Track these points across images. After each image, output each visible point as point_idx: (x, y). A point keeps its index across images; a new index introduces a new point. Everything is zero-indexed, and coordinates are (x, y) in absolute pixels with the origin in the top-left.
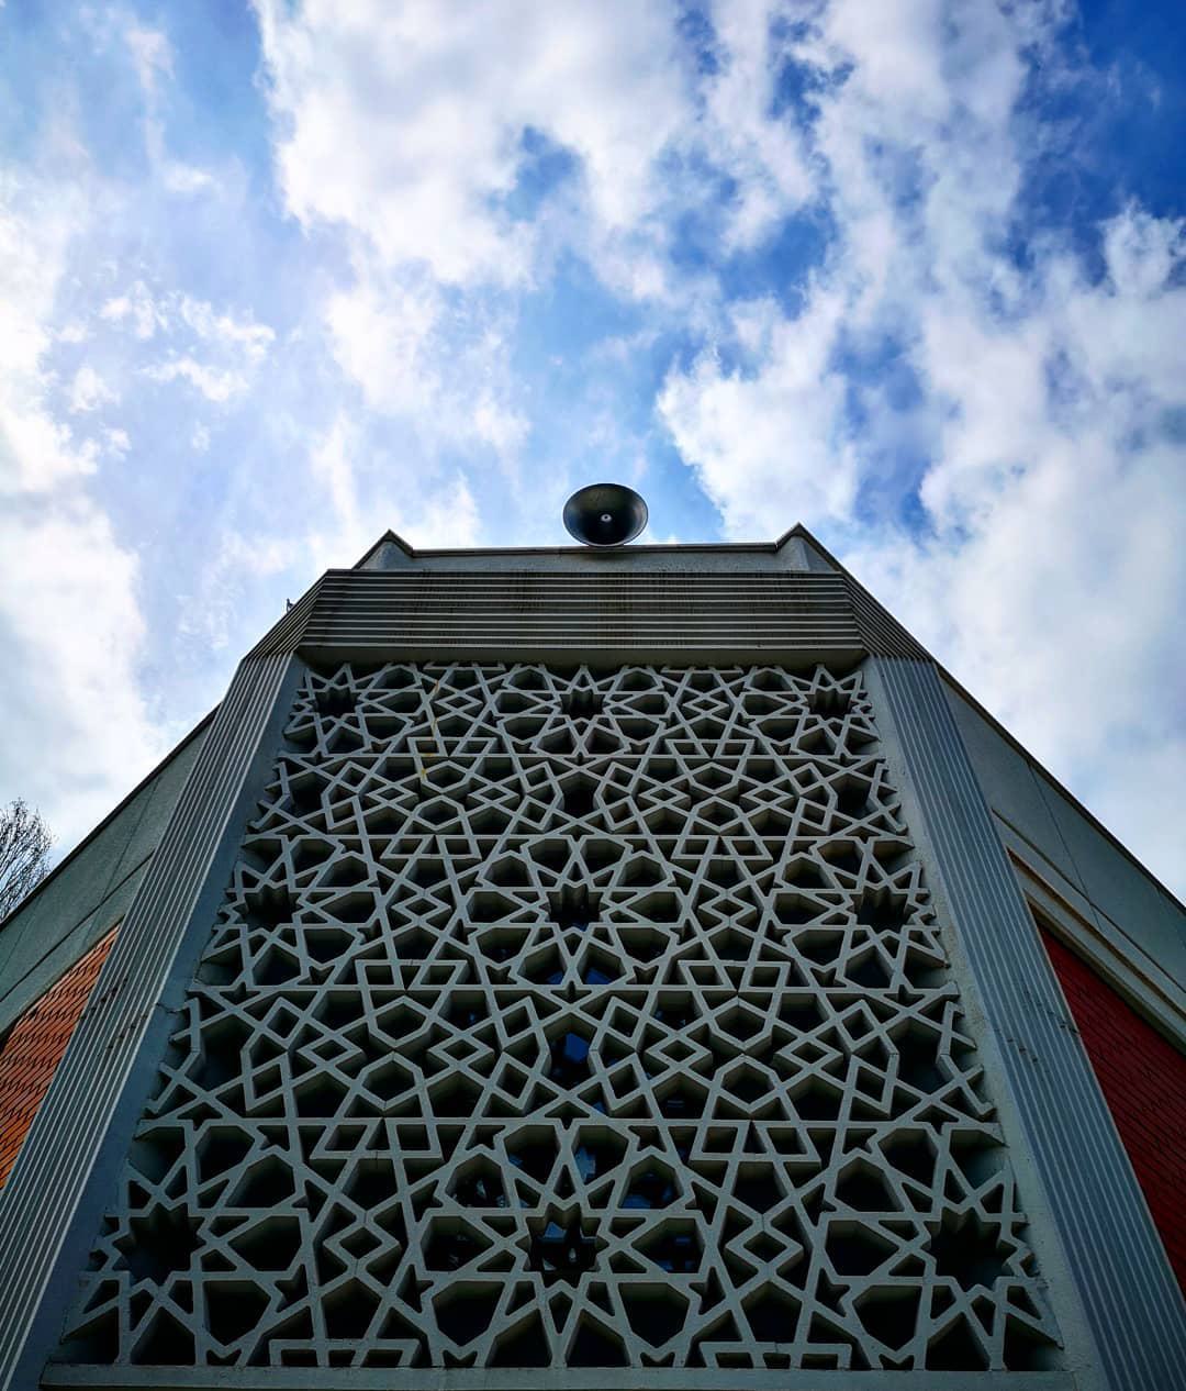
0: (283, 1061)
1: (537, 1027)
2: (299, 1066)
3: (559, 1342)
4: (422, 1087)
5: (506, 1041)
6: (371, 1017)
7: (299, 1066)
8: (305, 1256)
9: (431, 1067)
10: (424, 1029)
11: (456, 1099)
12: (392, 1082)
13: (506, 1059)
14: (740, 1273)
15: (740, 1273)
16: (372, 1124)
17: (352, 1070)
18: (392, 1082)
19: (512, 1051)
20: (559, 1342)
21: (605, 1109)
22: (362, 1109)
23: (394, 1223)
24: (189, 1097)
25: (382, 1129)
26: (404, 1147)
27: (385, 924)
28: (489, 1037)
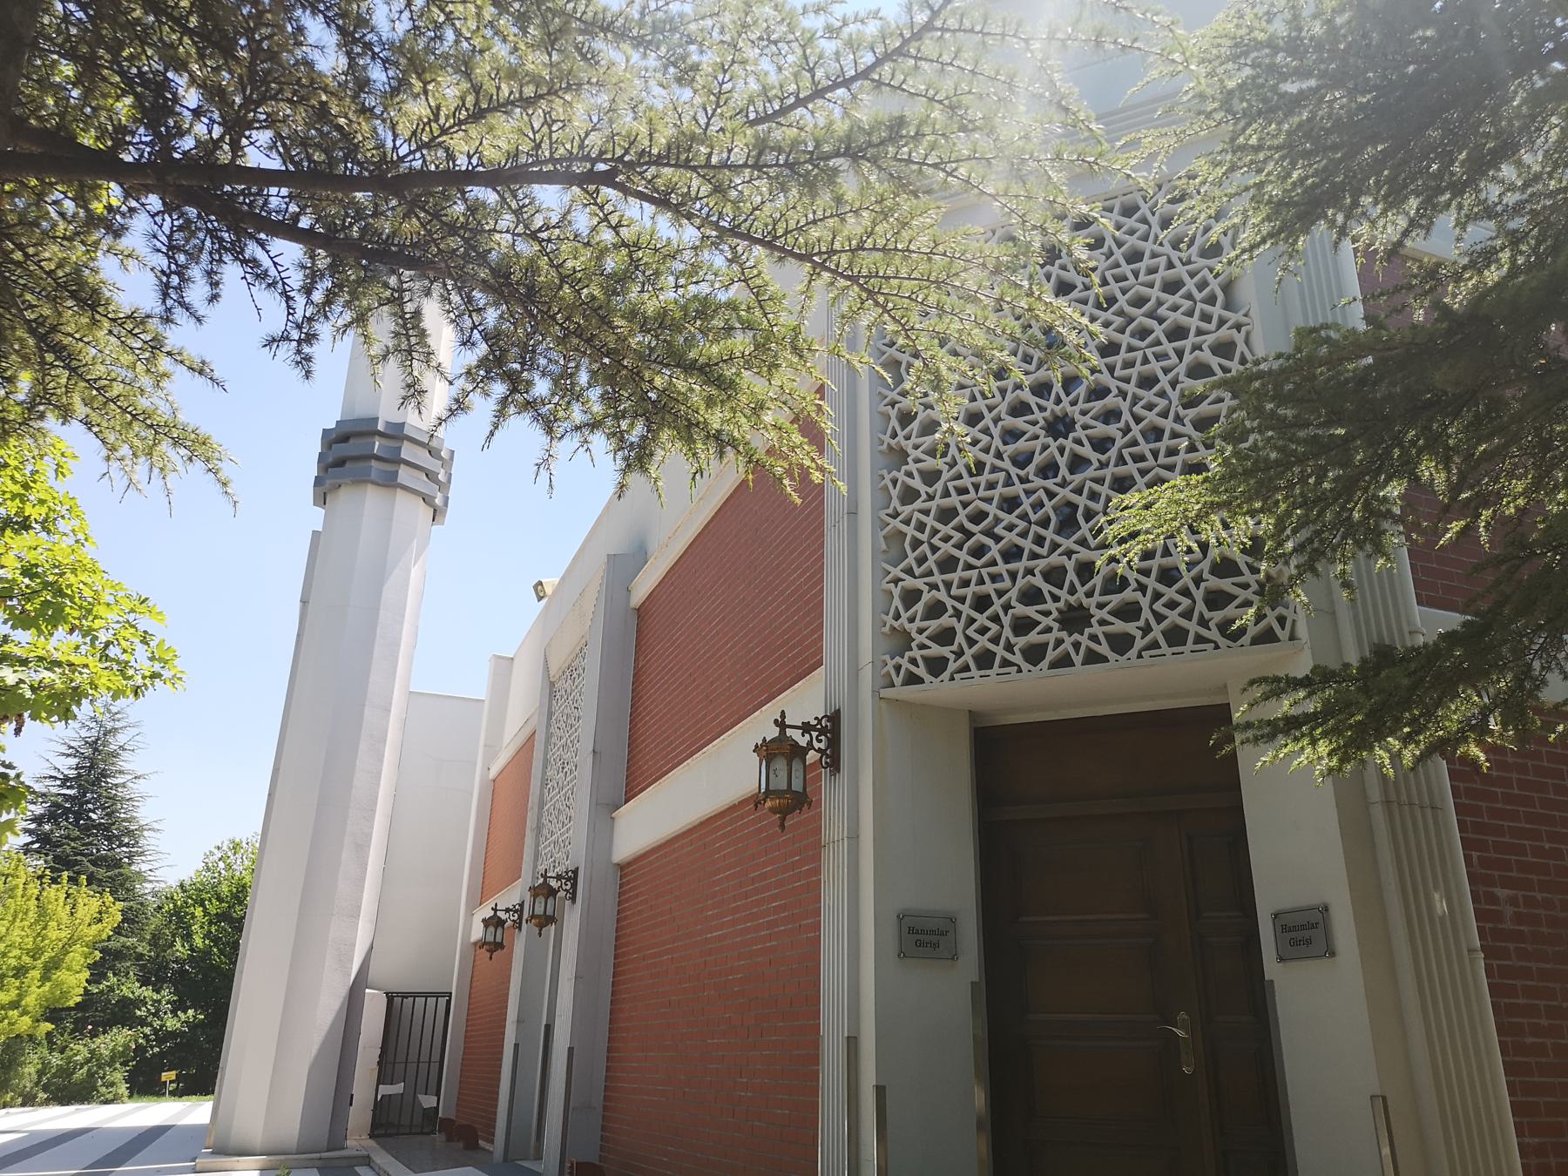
0: (925, 547)
1: (1048, 506)
2: (934, 549)
3: (1077, 659)
4: (995, 551)
5: (1198, 296)
6: (1122, 301)
7: (934, 549)
8: (960, 639)
9: (998, 539)
10: (990, 518)
11: (1012, 554)
12: (979, 552)
13: (1200, 305)
14: (1160, 618)
15: (1160, 618)
16: (1139, 354)
17: (959, 547)
18: (979, 552)
19: (1204, 301)
20: (1077, 659)
21: (1089, 548)
22: (1131, 349)
23: (995, 619)
24: (1141, 239)
25: (1145, 356)
26: (1007, 562)
27: (1114, 247)
28: (1189, 297)
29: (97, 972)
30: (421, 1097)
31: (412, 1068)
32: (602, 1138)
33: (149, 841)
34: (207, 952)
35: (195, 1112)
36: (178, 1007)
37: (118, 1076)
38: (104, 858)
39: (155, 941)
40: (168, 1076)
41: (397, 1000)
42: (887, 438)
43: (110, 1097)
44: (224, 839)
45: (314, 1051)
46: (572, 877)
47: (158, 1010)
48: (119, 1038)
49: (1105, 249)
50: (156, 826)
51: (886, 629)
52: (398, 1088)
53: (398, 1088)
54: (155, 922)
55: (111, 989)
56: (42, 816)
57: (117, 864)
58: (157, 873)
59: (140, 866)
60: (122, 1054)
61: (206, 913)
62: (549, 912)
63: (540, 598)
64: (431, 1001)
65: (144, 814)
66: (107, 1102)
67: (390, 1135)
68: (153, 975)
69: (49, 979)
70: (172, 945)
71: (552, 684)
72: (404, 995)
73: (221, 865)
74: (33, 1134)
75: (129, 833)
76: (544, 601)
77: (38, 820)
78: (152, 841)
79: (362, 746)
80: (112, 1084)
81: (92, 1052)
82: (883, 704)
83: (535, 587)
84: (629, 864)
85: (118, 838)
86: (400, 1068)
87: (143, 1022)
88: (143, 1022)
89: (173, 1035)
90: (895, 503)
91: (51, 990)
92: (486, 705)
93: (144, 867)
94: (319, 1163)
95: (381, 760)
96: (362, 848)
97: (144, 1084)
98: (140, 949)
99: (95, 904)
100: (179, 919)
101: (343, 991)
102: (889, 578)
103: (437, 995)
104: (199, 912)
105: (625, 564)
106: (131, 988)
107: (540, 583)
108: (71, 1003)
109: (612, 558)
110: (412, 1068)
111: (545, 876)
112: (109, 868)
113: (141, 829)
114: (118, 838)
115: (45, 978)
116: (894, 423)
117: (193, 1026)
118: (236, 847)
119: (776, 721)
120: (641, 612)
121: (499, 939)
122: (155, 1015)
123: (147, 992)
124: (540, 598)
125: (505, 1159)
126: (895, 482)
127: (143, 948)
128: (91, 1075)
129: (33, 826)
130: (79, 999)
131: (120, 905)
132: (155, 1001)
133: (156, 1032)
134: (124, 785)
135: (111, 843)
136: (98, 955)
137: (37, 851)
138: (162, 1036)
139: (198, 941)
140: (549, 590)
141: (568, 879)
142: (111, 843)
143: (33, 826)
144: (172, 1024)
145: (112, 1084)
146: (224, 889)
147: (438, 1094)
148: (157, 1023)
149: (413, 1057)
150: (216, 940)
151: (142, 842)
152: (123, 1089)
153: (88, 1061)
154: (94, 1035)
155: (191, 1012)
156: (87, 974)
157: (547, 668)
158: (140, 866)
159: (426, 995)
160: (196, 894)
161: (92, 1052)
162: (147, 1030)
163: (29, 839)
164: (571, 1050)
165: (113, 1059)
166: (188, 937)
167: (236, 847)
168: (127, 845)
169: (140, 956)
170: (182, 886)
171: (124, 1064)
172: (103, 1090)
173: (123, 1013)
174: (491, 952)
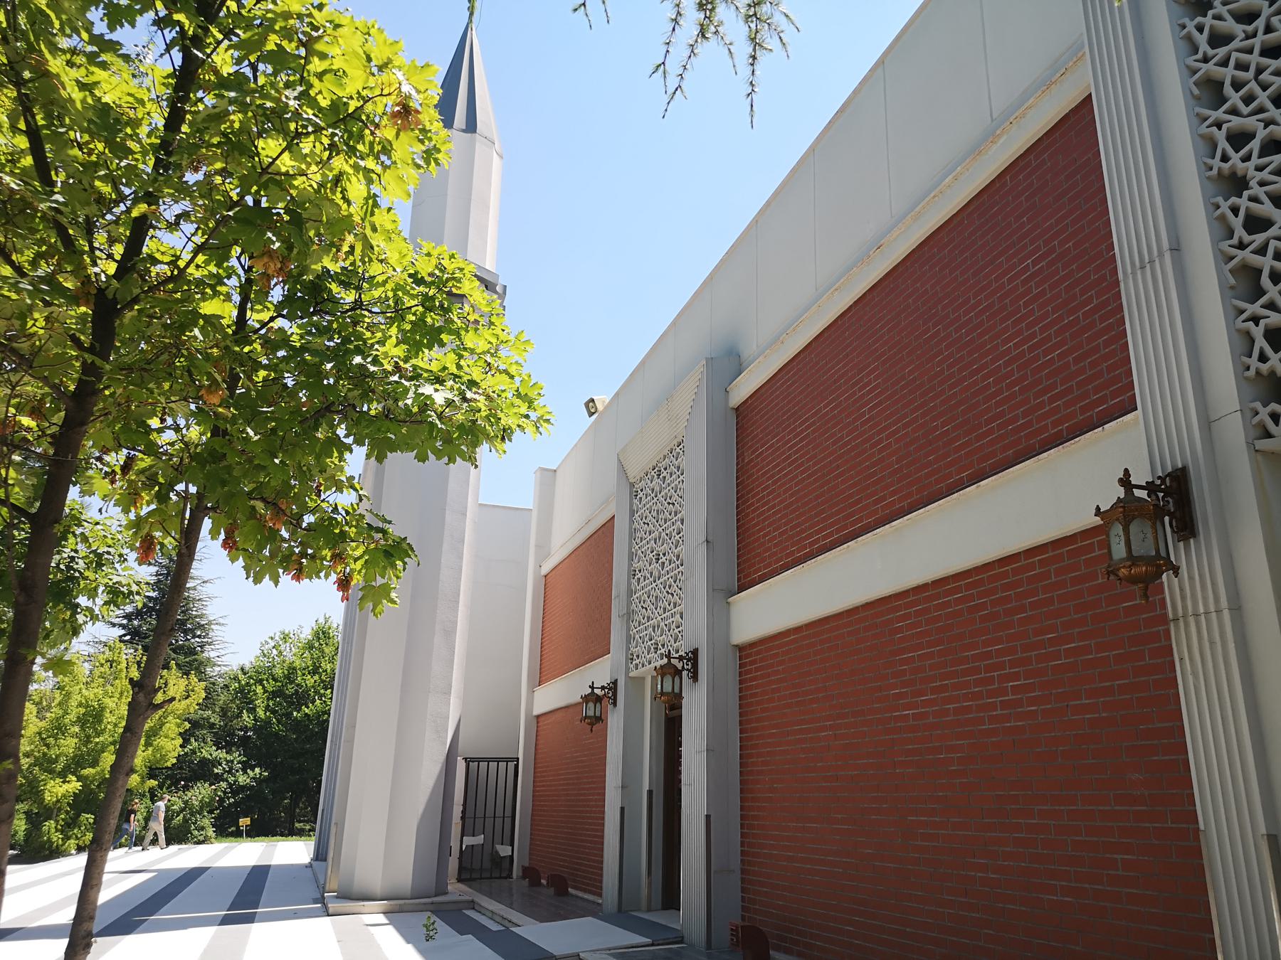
29: (186, 737)
30: (499, 847)
31: (489, 822)
32: (743, 899)
33: (216, 632)
34: (268, 722)
35: (292, 852)
36: (246, 767)
37: (206, 822)
38: (182, 647)
39: (224, 712)
40: (244, 822)
41: (473, 765)
42: (1216, 162)
43: (201, 838)
44: (275, 630)
45: (420, 808)
46: (693, 656)
47: (231, 769)
48: (201, 792)
49: (1250, 28)
50: (221, 621)
51: (1252, 373)
52: (479, 839)
53: (479, 839)
54: (223, 698)
55: (193, 752)
56: (132, 613)
57: (192, 652)
58: (223, 659)
59: (210, 653)
60: (209, 804)
61: (265, 691)
62: (677, 690)
63: (591, 414)
64: (493, 765)
65: (211, 611)
66: (199, 843)
67: (474, 880)
68: (224, 739)
69: (151, 745)
70: (239, 715)
71: (632, 485)
72: (479, 760)
73: (275, 652)
74: (161, 872)
75: (201, 627)
76: (595, 416)
77: (128, 617)
78: (218, 633)
79: (445, 547)
80: (203, 828)
81: (186, 803)
82: (1259, 457)
83: (587, 405)
84: (752, 645)
85: (192, 630)
86: (479, 823)
87: (219, 778)
88: (219, 778)
89: (243, 788)
90: (1240, 232)
91: (153, 754)
92: (535, 514)
93: (213, 654)
94: (431, 907)
95: (461, 558)
96: (450, 633)
97: (226, 828)
98: (212, 720)
99: (183, 683)
100: (244, 697)
101: (442, 758)
102: (1244, 316)
103: (507, 760)
104: (259, 689)
105: (729, 362)
106: (210, 752)
107: (592, 400)
108: (169, 764)
109: (710, 361)
110: (489, 822)
111: (669, 656)
112: (186, 655)
113: (210, 623)
114: (192, 630)
115: (148, 744)
116: (1223, 144)
117: (259, 781)
118: (285, 637)
119: (1121, 480)
120: (743, 412)
121: (598, 714)
122: (229, 772)
123: (222, 754)
124: (591, 414)
125: (620, 910)
126: (1235, 210)
127: (215, 719)
128: (185, 820)
129: (125, 622)
130: (174, 761)
131: (203, 684)
132: (228, 762)
133: (230, 785)
134: (194, 588)
135: (186, 634)
136: (187, 725)
137: (130, 642)
138: (236, 789)
139: (261, 713)
140: (600, 407)
141: (689, 660)
142: (186, 634)
143: (125, 622)
144: (242, 779)
145: (203, 828)
146: (278, 671)
147: (512, 845)
148: (231, 779)
149: (490, 812)
150: (274, 712)
151: (211, 634)
152: (210, 832)
153: (182, 810)
154: (186, 788)
155: (257, 770)
156: (180, 741)
157: (622, 469)
158: (210, 653)
159: (488, 760)
160: (258, 675)
161: (186, 803)
162: (224, 785)
163: (123, 632)
164: (708, 817)
165: (201, 808)
166: (252, 710)
167: (285, 637)
168: (199, 637)
169: (212, 726)
170: (242, 669)
171: (211, 812)
172: (196, 833)
173: (200, 771)
174: (592, 724)
